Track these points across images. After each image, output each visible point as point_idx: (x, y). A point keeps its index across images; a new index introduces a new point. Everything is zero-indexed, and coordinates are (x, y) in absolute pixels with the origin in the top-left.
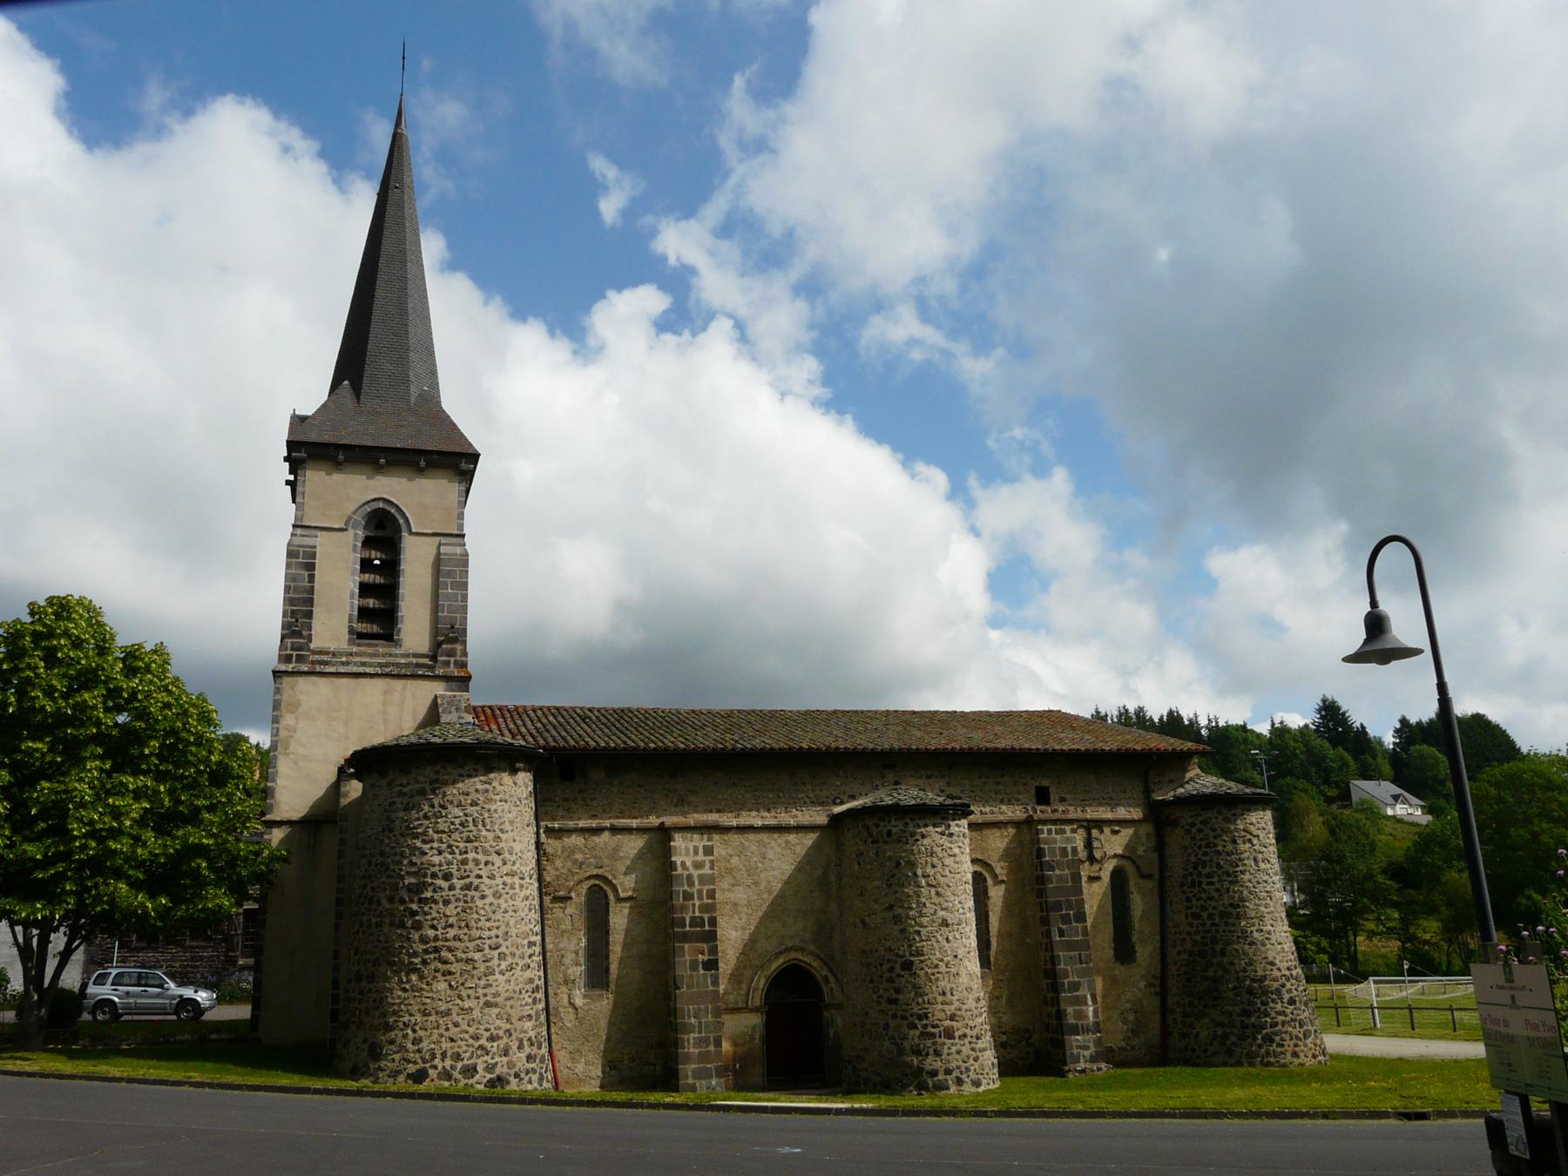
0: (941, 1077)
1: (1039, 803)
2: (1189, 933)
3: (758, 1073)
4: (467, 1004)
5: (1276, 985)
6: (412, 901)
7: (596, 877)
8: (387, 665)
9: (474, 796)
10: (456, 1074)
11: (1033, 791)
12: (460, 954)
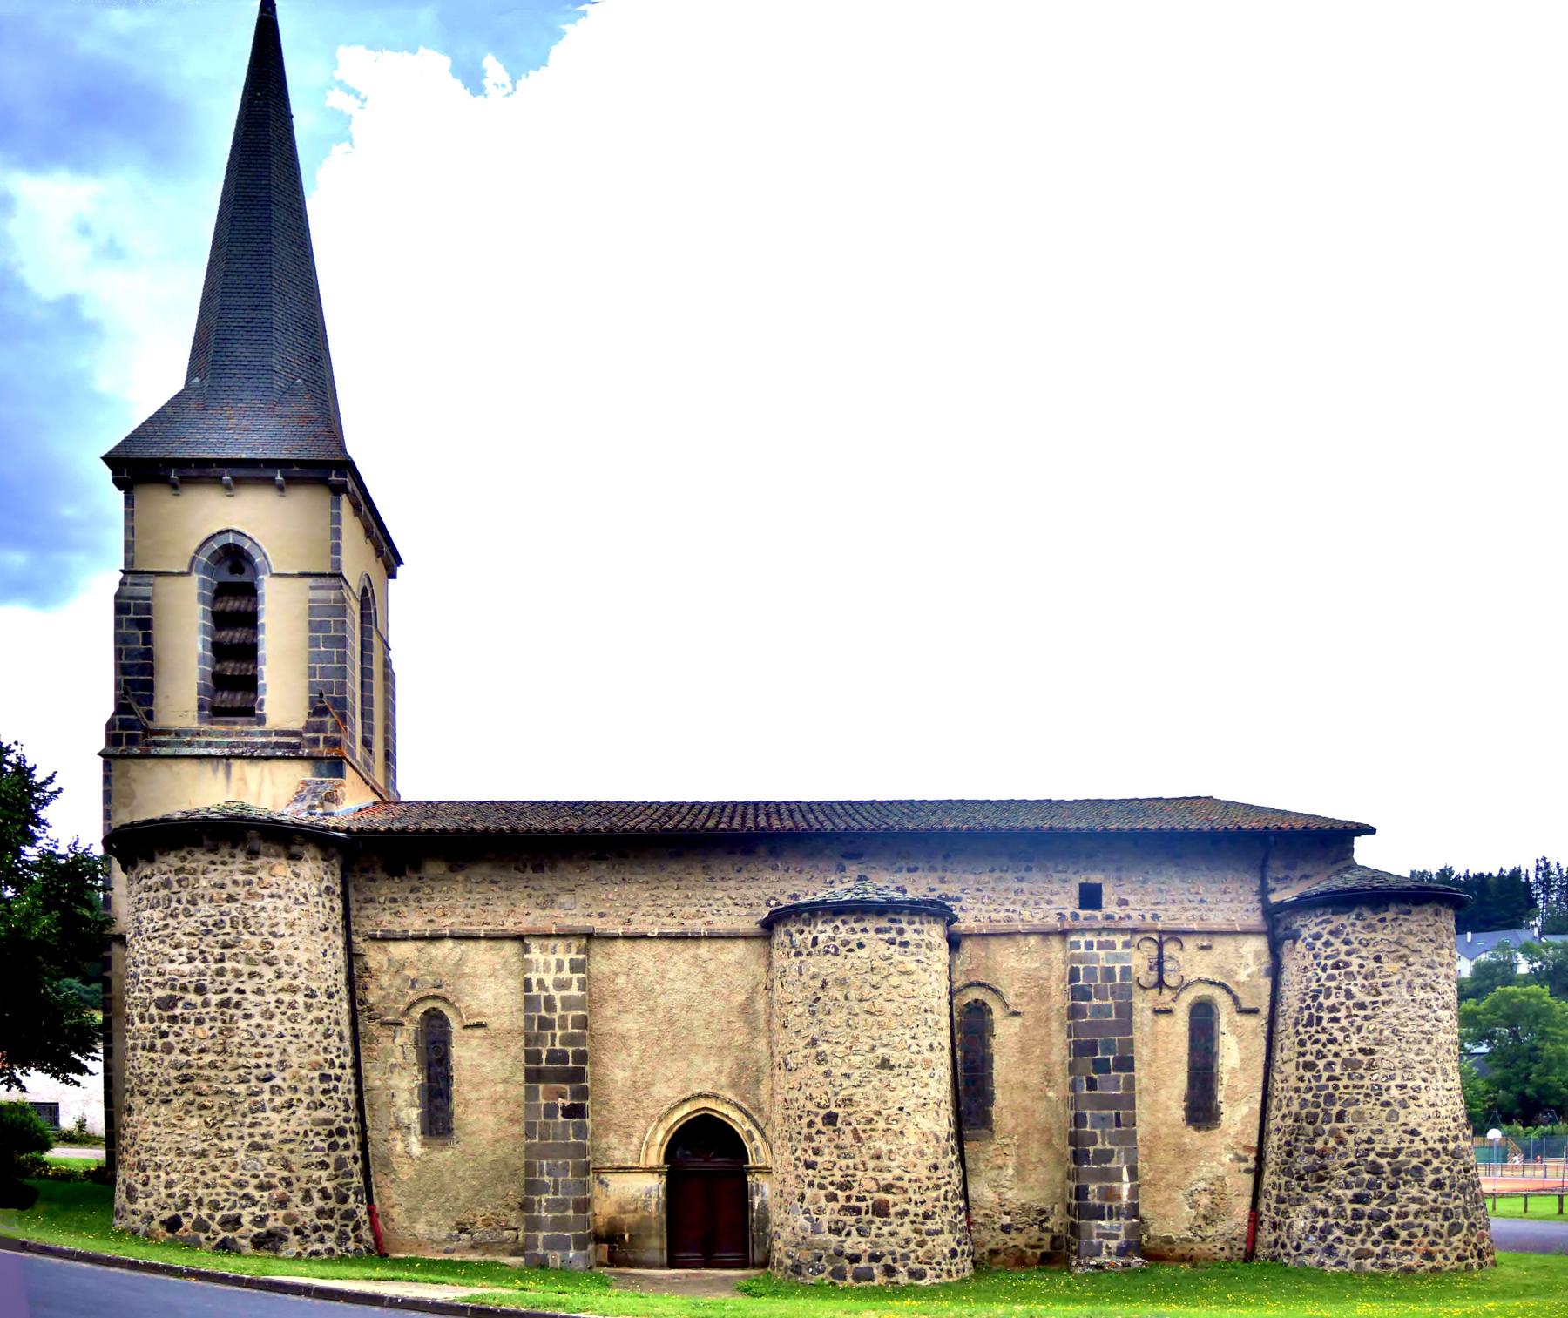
0: (863, 1264)
1: (1083, 906)
4: (226, 1145)
5: (1415, 1161)
6: (161, 1019)
7: (435, 997)
8: (237, 745)
9: (231, 889)
10: (215, 1226)
11: (1075, 892)
12: (217, 1085)
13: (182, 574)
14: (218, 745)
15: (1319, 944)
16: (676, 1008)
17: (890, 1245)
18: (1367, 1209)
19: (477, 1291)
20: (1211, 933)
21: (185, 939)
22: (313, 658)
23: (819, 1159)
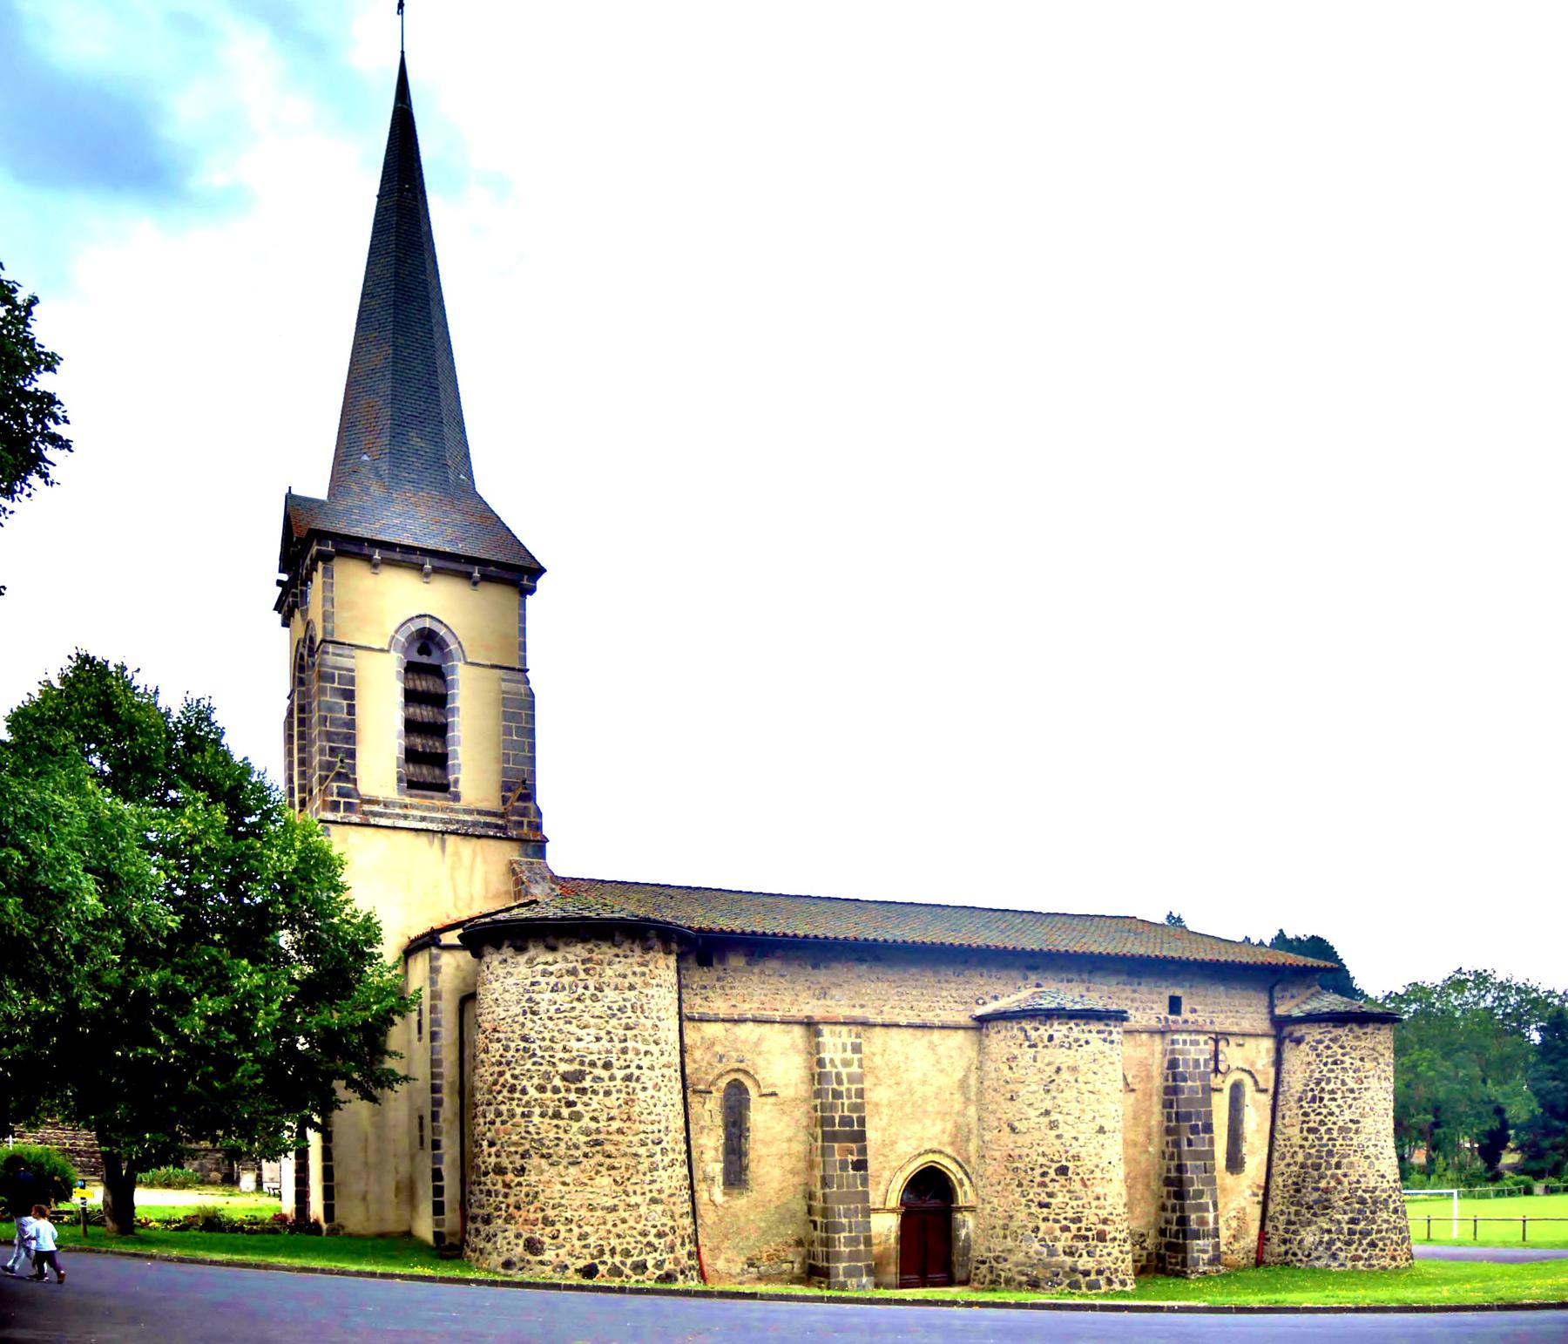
0: (1093, 1277)
2: (1302, 1147)
3: (892, 1271)
4: (633, 1200)
5: (1385, 1196)
6: (568, 1090)
7: (738, 1070)
8: (450, 822)
9: (631, 979)
10: (627, 1271)
11: (1167, 1002)
12: (623, 1148)
13: (382, 650)
14: (432, 820)
15: (1321, 1047)
16: (919, 1081)
17: (1107, 1263)
18: (1358, 1228)
19: (1265, 1297)
20: (1244, 1035)
21: (592, 1021)
22: (507, 745)
23: (1052, 1200)
